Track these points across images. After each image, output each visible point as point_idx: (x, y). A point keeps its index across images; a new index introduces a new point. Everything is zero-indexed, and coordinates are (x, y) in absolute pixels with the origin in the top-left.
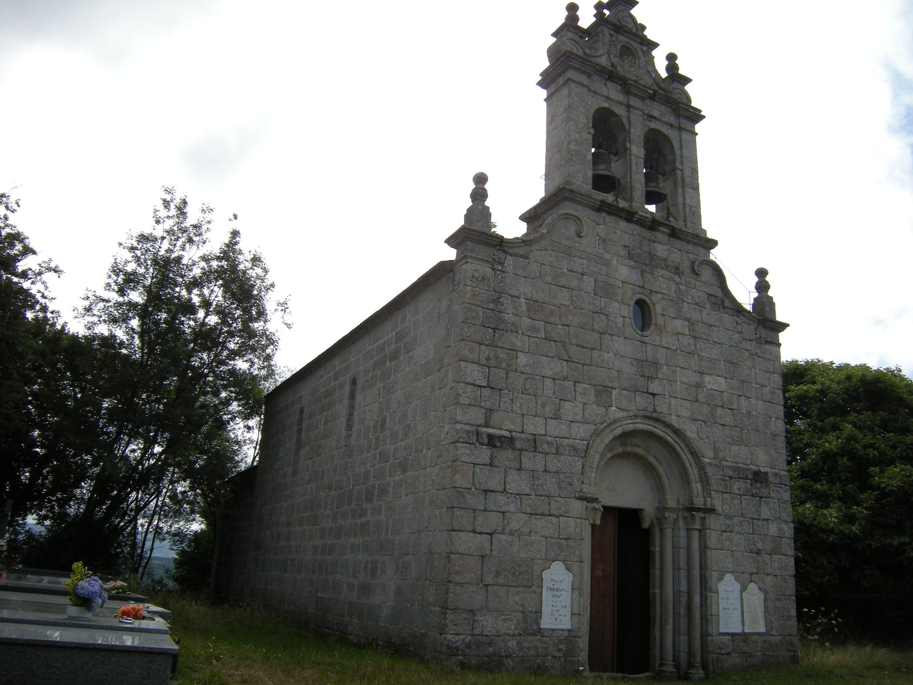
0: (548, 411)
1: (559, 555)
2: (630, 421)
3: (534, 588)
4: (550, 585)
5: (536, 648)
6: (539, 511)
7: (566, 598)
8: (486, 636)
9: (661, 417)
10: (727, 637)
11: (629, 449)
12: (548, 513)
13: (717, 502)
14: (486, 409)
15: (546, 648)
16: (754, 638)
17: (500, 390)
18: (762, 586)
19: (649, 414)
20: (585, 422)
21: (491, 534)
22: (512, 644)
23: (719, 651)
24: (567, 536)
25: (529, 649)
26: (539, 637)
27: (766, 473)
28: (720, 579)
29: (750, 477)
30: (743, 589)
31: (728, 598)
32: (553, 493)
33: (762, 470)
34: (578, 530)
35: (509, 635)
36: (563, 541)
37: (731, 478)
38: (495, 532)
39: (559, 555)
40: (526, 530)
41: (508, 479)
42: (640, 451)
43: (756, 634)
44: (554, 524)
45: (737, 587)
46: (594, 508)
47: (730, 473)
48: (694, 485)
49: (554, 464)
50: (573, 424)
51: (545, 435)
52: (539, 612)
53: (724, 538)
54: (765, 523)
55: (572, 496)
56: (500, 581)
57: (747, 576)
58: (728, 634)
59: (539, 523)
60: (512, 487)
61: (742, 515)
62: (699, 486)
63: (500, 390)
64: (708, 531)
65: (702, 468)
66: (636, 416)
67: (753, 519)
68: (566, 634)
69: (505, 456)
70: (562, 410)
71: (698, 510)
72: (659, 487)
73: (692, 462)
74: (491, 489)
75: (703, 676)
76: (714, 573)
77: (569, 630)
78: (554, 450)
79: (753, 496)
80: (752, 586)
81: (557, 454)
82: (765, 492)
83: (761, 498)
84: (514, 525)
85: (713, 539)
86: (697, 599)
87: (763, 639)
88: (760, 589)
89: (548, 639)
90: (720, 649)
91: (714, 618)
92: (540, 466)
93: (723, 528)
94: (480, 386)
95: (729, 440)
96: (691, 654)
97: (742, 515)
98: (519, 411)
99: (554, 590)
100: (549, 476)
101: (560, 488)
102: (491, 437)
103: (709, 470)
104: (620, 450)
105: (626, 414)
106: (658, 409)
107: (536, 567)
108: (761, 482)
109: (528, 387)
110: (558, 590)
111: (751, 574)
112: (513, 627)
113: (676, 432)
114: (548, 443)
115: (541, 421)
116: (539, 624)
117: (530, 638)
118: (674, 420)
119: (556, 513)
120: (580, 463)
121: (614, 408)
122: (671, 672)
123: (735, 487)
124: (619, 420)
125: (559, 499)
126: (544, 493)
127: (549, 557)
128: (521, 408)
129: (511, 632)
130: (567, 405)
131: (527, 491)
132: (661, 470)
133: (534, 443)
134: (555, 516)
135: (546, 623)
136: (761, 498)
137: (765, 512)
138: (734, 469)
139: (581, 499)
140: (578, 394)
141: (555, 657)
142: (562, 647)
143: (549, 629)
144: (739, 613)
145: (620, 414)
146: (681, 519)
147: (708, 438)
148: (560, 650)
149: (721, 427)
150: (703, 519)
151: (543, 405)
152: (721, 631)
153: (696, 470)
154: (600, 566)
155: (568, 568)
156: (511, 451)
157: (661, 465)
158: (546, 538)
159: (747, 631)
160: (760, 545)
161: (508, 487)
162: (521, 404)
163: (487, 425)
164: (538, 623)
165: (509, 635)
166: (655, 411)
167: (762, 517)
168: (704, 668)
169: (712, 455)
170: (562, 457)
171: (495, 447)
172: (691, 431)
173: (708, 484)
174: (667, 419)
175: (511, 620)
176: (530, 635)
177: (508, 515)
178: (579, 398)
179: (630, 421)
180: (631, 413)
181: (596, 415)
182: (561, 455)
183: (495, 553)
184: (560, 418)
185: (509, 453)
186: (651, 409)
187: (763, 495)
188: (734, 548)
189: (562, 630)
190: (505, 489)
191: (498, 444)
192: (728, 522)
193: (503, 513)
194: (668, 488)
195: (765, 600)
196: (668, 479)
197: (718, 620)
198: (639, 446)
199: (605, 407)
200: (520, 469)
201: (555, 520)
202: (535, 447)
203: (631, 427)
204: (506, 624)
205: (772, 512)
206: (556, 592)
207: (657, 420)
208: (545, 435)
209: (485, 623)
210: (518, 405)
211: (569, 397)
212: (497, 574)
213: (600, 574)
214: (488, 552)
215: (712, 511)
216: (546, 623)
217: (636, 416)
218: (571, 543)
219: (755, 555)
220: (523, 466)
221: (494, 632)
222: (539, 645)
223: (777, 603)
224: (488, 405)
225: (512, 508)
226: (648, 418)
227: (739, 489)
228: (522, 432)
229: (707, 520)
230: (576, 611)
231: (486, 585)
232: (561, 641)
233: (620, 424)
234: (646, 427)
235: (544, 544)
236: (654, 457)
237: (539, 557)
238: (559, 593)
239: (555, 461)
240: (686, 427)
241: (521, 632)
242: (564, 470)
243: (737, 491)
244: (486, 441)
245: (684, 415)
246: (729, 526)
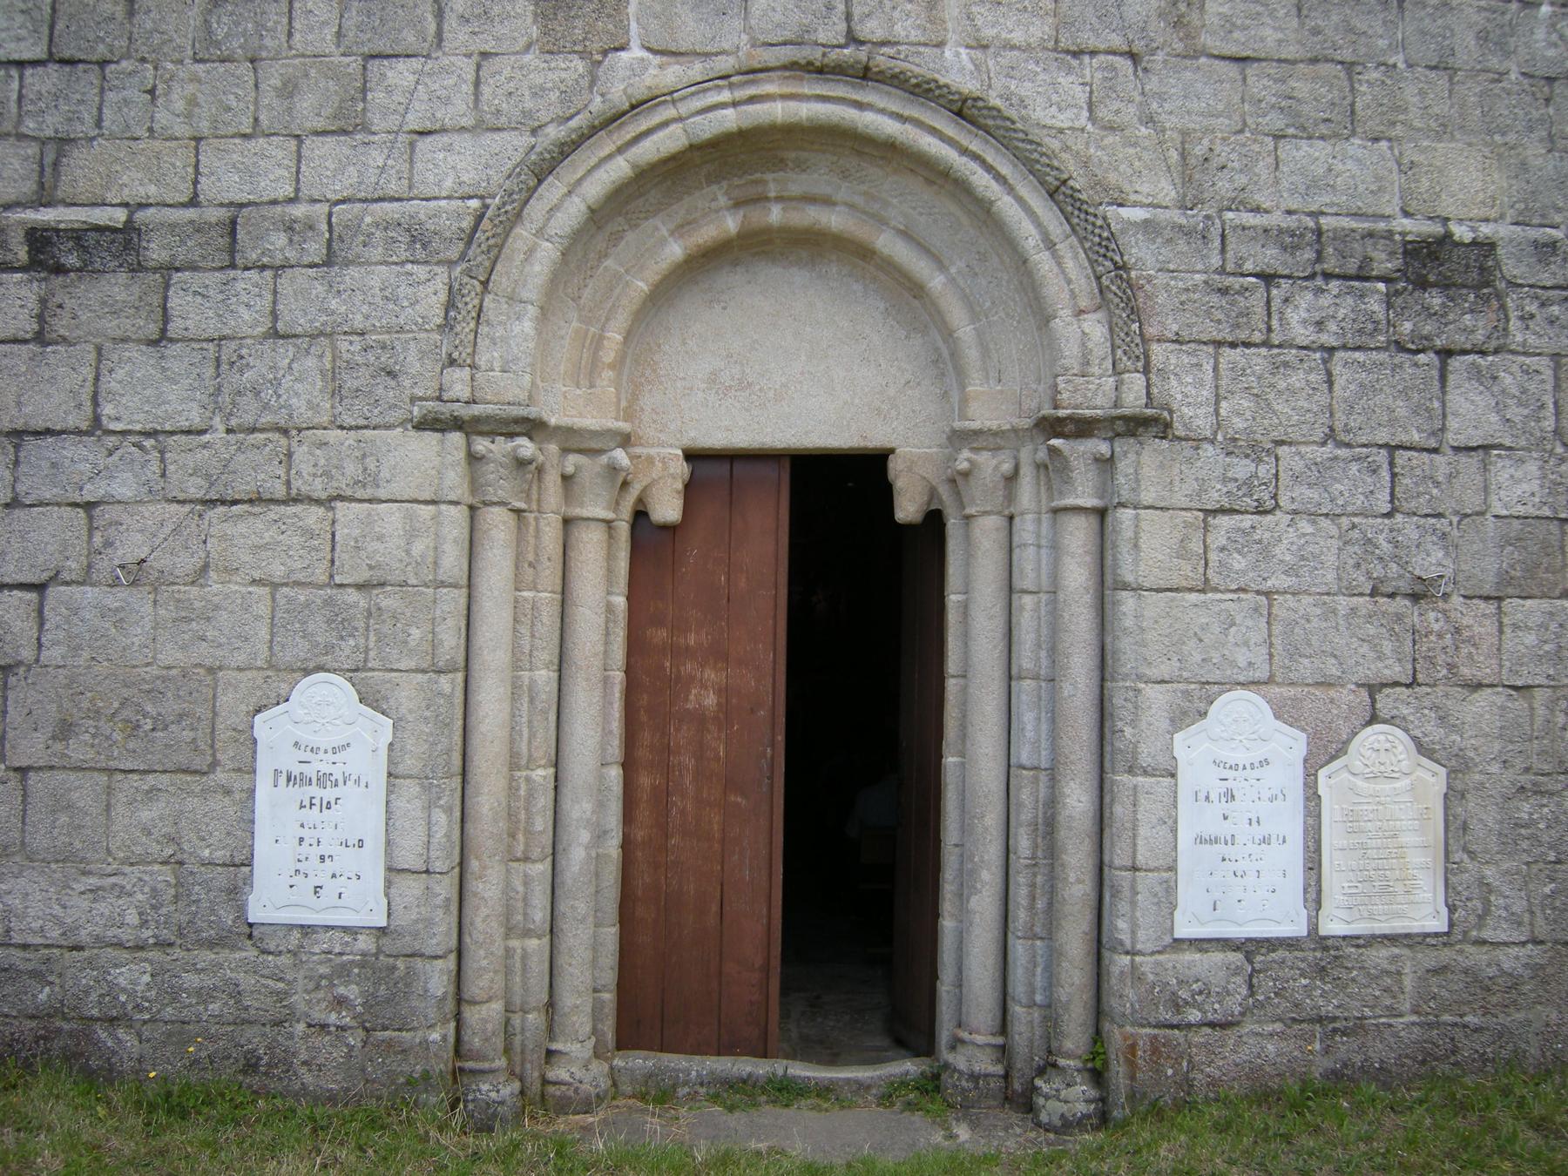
0: (310, 108)
1: (329, 649)
2: (725, 96)
3: (220, 776)
4: (290, 763)
5: (237, 994)
6: (242, 488)
7: (361, 810)
8: (25, 947)
9: (881, 61)
10: (1217, 957)
11: (775, 215)
12: (280, 491)
13: (1188, 391)
14: (43, 142)
15: (281, 996)
16: (1380, 956)
17: (103, 63)
18: (1434, 733)
19: (816, 55)
20: (482, 127)
21: (40, 588)
22: (132, 977)
23: (1167, 1016)
24: (363, 575)
25: (205, 995)
26: (252, 953)
27: (1487, 247)
28: (1188, 714)
29: (1385, 263)
30: (1325, 750)
31: (1230, 796)
32: (302, 413)
33: (1462, 233)
34: (418, 547)
35: (119, 945)
36: (352, 596)
37: (1268, 278)
38: (55, 578)
39: (329, 649)
40: (187, 563)
41: (110, 383)
42: (834, 220)
43: (1392, 939)
44: (310, 534)
45: (1290, 745)
46: (521, 463)
47: (1270, 257)
48: (1064, 324)
49: (304, 298)
50: (424, 144)
51: (291, 201)
52: (244, 863)
53: (1218, 539)
54: (1470, 463)
55: (399, 415)
56: (78, 750)
57: (1350, 698)
58: (1225, 944)
59: (242, 533)
60: (123, 411)
61: (1330, 435)
62: (1095, 328)
63: (103, 63)
64: (1126, 515)
65: (1103, 249)
66: (753, 72)
67: (1392, 449)
68: (365, 943)
69: (99, 303)
70: (377, 96)
71: (1083, 428)
72: (946, 363)
73: (1056, 226)
74: (40, 424)
75: (1081, 1108)
76: (1150, 691)
77: (382, 931)
78: (315, 249)
79: (1400, 347)
80: (1380, 746)
81: (328, 262)
82: (1473, 325)
83: (1446, 353)
84: (131, 547)
85: (1150, 546)
86: (1077, 800)
87: (1429, 959)
88: (1423, 749)
89: (285, 960)
90: (1177, 1005)
91: (1147, 882)
92: (248, 317)
93: (1214, 498)
94: (21, 64)
95: (1277, 122)
96: (1051, 1016)
97: (1330, 435)
98: (181, 129)
99: (304, 780)
100: (286, 351)
101: (336, 393)
102: (39, 239)
103: (1141, 254)
104: (731, 224)
105: (697, 70)
106: (871, 29)
107: (225, 700)
108: (1445, 286)
109: (220, 34)
110: (323, 780)
111: (1373, 689)
112: (132, 918)
113: (964, 109)
114: (289, 227)
115: (279, 151)
116: (242, 910)
117: (206, 957)
118: (957, 68)
119: (318, 489)
120: (440, 284)
121: (636, 52)
122: (974, 1077)
123: (1294, 317)
124: (668, 96)
125: (334, 435)
126: (267, 419)
127: (286, 657)
128: (189, 116)
129: (126, 935)
130: (400, 74)
131: (195, 417)
132: (936, 282)
133: (229, 240)
134: (318, 502)
135: (272, 900)
136: (1446, 353)
137: (1471, 410)
138: (1289, 240)
139: (424, 425)
140: (451, 22)
141: (324, 1027)
142: (352, 991)
143: (291, 927)
144: (1292, 856)
145: (672, 74)
146: (1027, 474)
147: (1150, 120)
148: (340, 1002)
149: (1232, 70)
150: (1107, 464)
151: (289, 90)
152: (1183, 930)
153: (1075, 264)
154: (710, 674)
155: (370, 699)
156: (123, 277)
157: (940, 264)
158: (275, 586)
159: (1332, 926)
160: (1431, 561)
161: (107, 409)
162: (192, 102)
163: (44, 198)
164: (236, 893)
165: (119, 945)
166: (852, 39)
167: (1451, 438)
168: (1098, 1076)
169: (1167, 191)
170: (353, 272)
171: (60, 270)
172: (1051, 102)
173: (1135, 313)
174: (920, 65)
175: (122, 892)
176: (211, 945)
177: (105, 514)
178: (457, 35)
179: (725, 96)
180: (725, 64)
181: (538, 92)
182: (348, 263)
183: (53, 654)
184: (365, 128)
185: (118, 287)
186: (831, 32)
187: (1460, 340)
188: (1278, 581)
189: (345, 929)
190: (96, 420)
191: (72, 260)
192: (1242, 468)
193: (89, 506)
194: (972, 354)
195: (1453, 796)
196: (974, 317)
197: (1170, 889)
198: (827, 202)
199: (583, 55)
200: (161, 339)
201: (313, 516)
202: (232, 249)
203: (729, 120)
204: (102, 907)
205: (1515, 412)
206: (314, 790)
207: (865, 74)
208: (291, 201)
209: (17, 903)
210: (179, 106)
211: (410, 39)
212: (65, 730)
213: (711, 700)
214: (27, 654)
215: (1147, 424)
216: (272, 900)
217: (753, 72)
218: (388, 600)
219: (1401, 604)
220: (175, 328)
221: (54, 934)
222: (247, 981)
223: (1525, 809)
224: (52, 124)
225: (124, 486)
226: (821, 71)
227: (1320, 325)
228: (193, 202)
229: (1124, 466)
230: (409, 857)
231: (22, 771)
232: (343, 972)
233: (670, 112)
234: (805, 111)
235: (263, 609)
236: (906, 234)
237: (241, 658)
238: (329, 794)
239: (319, 289)
240: (1026, 89)
241: (166, 934)
242: (358, 322)
243: (1303, 334)
244: (23, 254)
245: (1017, 37)
246: (1248, 484)
